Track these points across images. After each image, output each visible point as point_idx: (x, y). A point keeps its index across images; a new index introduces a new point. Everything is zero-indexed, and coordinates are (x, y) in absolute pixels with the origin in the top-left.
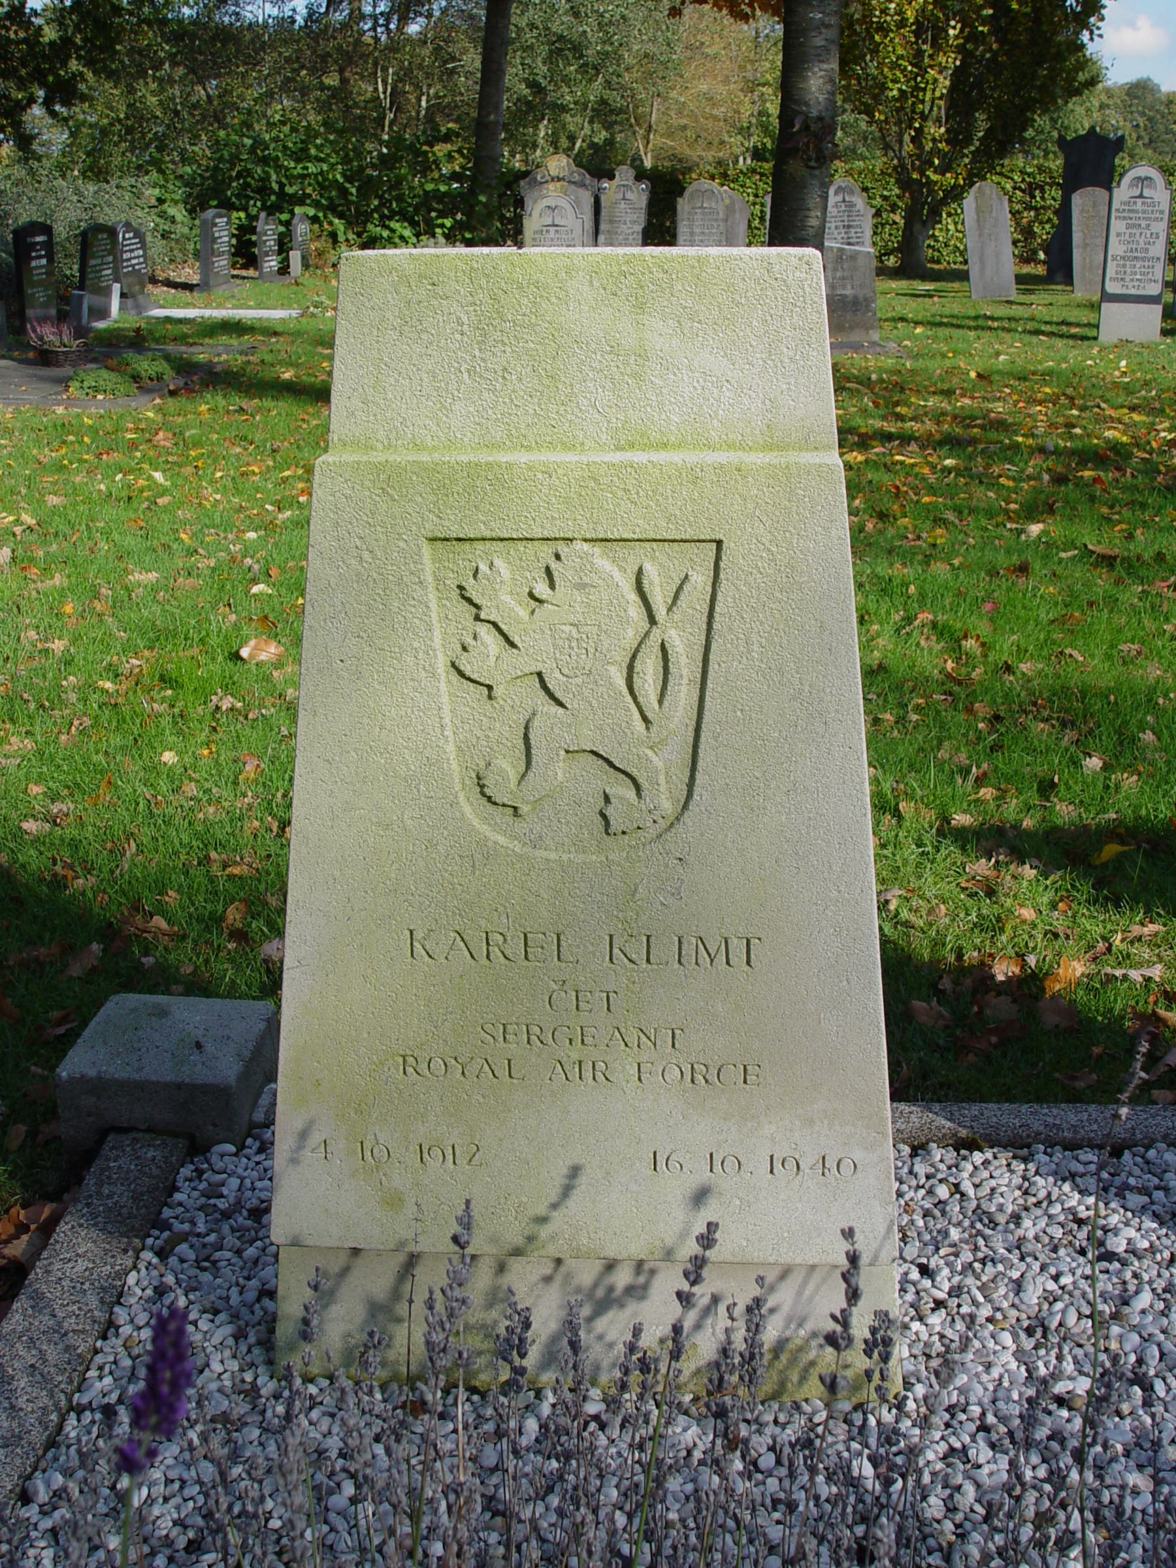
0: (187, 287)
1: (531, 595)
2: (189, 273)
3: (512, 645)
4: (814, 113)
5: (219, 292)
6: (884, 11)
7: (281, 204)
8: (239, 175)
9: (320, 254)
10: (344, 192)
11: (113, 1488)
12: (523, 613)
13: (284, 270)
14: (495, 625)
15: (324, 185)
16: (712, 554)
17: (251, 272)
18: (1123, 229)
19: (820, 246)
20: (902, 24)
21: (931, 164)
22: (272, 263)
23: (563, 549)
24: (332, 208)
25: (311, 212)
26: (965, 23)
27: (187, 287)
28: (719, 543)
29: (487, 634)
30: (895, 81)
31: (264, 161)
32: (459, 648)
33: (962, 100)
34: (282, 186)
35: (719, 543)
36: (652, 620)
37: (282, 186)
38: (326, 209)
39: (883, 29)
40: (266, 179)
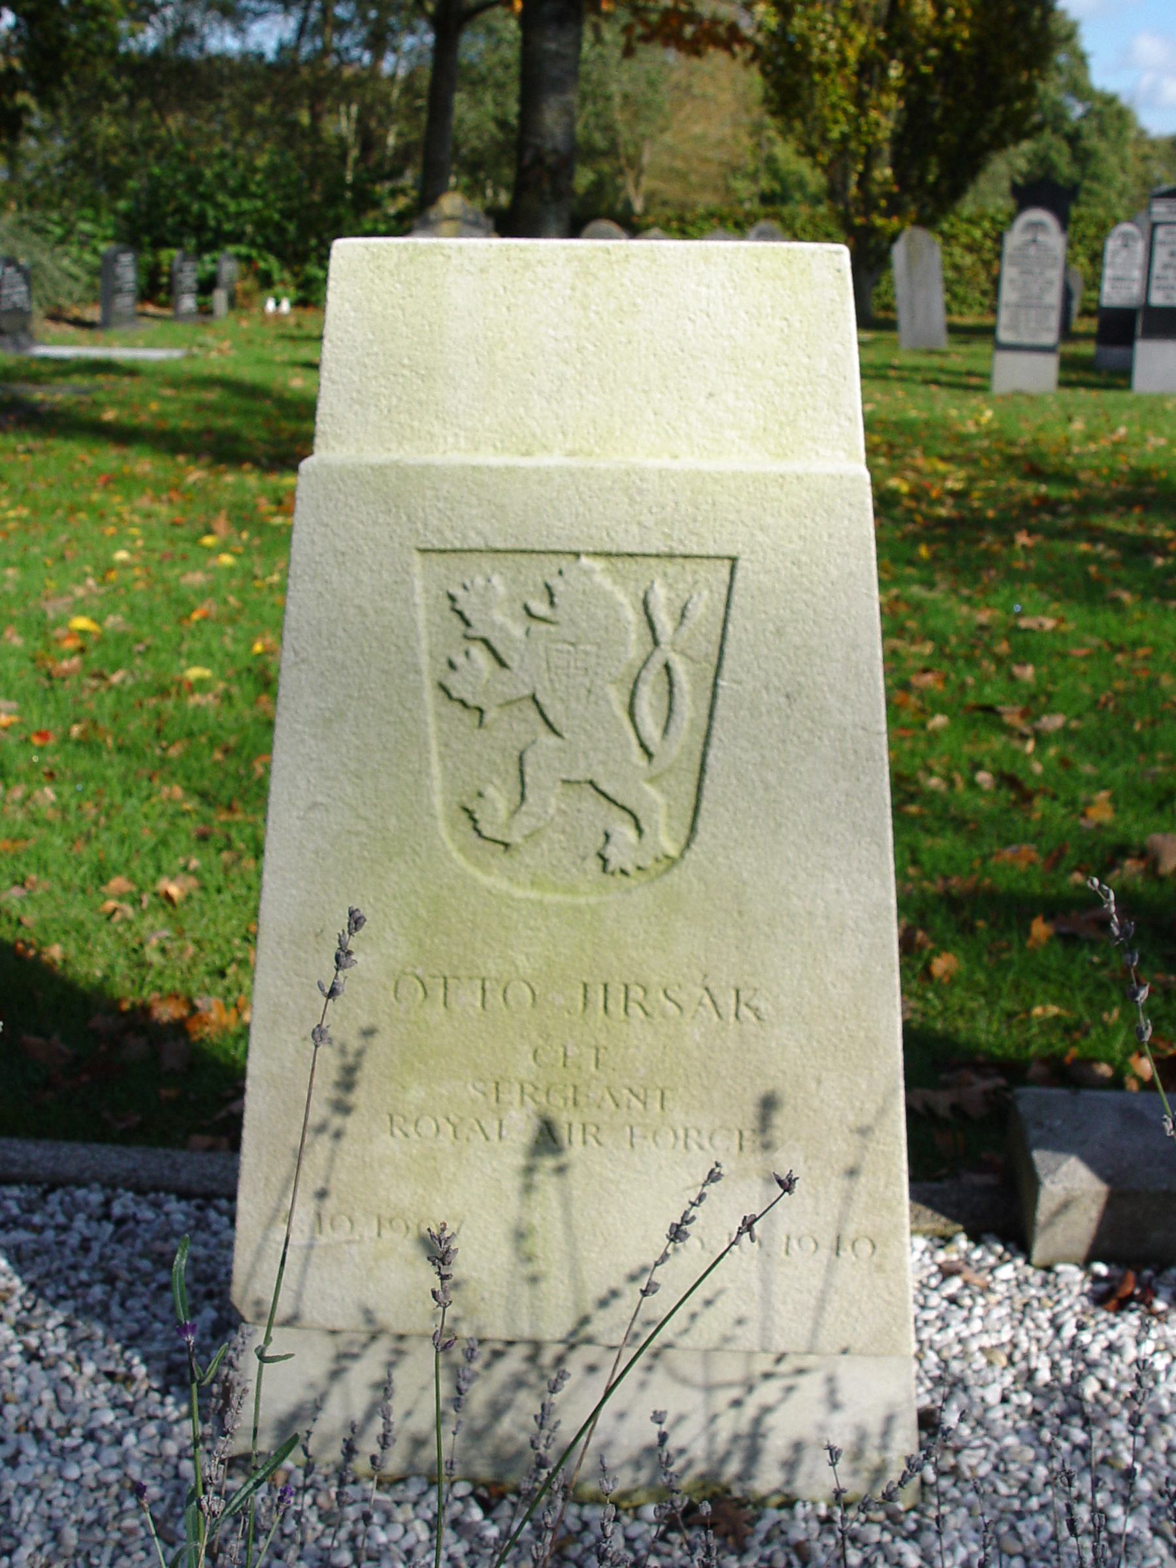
0: (89, 325)
1: (527, 609)
2: (93, 313)
3: (502, 664)
4: (549, 146)
5: (114, 332)
6: (824, 50)
7: (211, 241)
8: (176, 211)
9: (247, 294)
10: (281, 230)
11: (92, 1490)
12: (518, 631)
13: (205, 311)
14: (485, 641)
15: (261, 224)
16: (725, 573)
17: (167, 312)
18: (4, 831)
19: (1117, 221)
20: (843, 63)
21: (876, 207)
22: (188, 303)
23: (565, 562)
24: (269, 247)
25: (243, 250)
26: (908, 62)
27: (89, 325)
28: (734, 560)
29: (479, 654)
30: (836, 122)
31: (203, 197)
32: (446, 667)
33: (911, 142)
34: (219, 222)
35: (734, 560)
36: (656, 643)
37: (219, 222)
38: (258, 247)
39: (824, 69)
40: (202, 215)
